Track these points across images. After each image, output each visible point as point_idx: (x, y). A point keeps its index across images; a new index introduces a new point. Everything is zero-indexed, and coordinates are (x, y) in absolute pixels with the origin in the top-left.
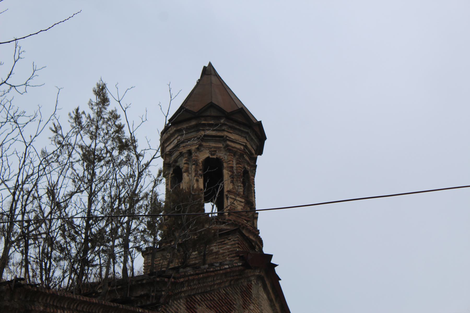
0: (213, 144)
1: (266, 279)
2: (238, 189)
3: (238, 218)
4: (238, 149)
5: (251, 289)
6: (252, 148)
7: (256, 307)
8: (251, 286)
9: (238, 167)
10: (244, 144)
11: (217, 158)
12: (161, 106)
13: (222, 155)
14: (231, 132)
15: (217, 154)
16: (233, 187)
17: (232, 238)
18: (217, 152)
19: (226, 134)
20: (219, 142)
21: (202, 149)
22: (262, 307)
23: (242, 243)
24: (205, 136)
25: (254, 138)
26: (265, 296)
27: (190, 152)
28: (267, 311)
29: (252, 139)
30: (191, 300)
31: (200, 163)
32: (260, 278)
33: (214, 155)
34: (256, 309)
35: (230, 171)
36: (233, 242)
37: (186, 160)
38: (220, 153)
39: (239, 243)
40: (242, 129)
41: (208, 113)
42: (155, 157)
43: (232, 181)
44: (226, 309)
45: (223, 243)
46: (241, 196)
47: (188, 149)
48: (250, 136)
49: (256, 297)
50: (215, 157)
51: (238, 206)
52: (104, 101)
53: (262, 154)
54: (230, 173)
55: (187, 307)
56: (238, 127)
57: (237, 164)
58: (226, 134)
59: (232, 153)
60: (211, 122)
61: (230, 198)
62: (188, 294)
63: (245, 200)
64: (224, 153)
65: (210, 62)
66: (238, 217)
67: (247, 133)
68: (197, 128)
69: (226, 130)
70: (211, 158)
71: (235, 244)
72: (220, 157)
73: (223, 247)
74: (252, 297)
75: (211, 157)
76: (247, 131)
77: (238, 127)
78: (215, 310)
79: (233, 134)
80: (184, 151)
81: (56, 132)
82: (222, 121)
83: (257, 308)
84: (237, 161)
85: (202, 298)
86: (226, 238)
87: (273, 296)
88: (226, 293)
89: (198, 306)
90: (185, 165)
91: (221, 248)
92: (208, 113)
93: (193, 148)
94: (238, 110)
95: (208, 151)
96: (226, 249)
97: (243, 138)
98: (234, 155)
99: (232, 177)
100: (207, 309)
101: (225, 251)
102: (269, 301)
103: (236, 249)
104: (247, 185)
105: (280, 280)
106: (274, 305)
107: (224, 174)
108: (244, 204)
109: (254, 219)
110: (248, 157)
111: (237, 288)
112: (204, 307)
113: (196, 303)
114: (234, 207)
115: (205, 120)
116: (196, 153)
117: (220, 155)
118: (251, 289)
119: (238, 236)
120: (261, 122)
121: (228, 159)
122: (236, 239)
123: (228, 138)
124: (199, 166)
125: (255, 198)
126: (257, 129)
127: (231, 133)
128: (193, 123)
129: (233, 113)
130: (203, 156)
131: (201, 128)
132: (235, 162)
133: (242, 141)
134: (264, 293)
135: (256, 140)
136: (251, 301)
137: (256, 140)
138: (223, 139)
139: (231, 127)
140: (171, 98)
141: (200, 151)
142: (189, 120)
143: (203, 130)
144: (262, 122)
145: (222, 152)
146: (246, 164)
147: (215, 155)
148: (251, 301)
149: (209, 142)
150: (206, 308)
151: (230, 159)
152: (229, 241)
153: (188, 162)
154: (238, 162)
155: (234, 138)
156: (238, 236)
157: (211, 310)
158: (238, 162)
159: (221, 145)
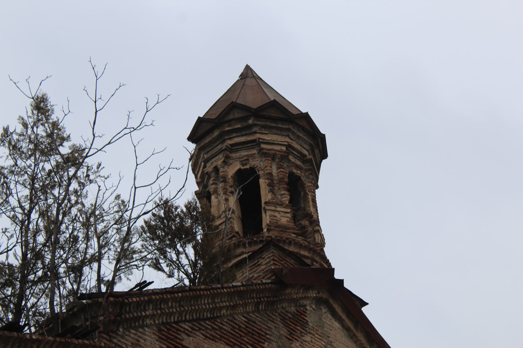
0: (244, 153)
1: (331, 302)
2: (281, 198)
3: (283, 233)
5: (306, 316)
6: (302, 148)
7: (318, 338)
8: (306, 313)
9: (279, 172)
10: (286, 144)
11: (250, 167)
12: (86, 91)
13: (257, 162)
14: (267, 132)
15: (250, 163)
16: (272, 197)
17: (266, 256)
18: (250, 160)
19: (258, 136)
20: (252, 148)
21: (231, 161)
22: (330, 339)
23: (282, 259)
24: (232, 145)
25: (301, 135)
26: (337, 325)
27: (216, 169)
28: (343, 344)
29: (299, 137)
30: (168, 329)
31: (230, 179)
32: (319, 302)
33: (246, 164)
34: (317, 341)
35: (268, 179)
36: (268, 260)
37: (213, 180)
38: (254, 161)
39: (276, 259)
40: (280, 126)
41: (231, 117)
43: (270, 189)
44: (247, 341)
46: (285, 206)
47: (214, 166)
48: (293, 133)
49: (317, 326)
50: (248, 167)
51: (282, 218)
53: (327, 156)
54: (267, 181)
55: (160, 337)
56: (273, 125)
57: (278, 168)
58: (258, 136)
59: (268, 157)
60: (236, 127)
61: (269, 210)
62: (163, 322)
63: (291, 209)
64: (259, 160)
66: (281, 231)
67: (289, 130)
68: (221, 138)
69: (258, 131)
70: (243, 169)
71: (269, 262)
72: (254, 165)
73: (257, 270)
74: (307, 326)
75: (242, 168)
76: (287, 127)
77: (273, 125)
78: (225, 342)
79: (269, 135)
82: (250, 122)
83: (320, 339)
84: (278, 165)
85: (193, 326)
86: (261, 257)
88: (248, 319)
89: (185, 337)
90: (212, 186)
91: (254, 272)
92: (231, 117)
93: (220, 163)
94: (270, 102)
96: (260, 271)
97: (283, 137)
98: (273, 159)
99: (271, 185)
100: (206, 341)
101: (260, 274)
102: (345, 331)
103: (271, 267)
104: (302, 195)
105: (365, 304)
106: (354, 335)
107: (260, 184)
108: (291, 215)
110: (299, 160)
111: (273, 314)
112: (198, 338)
113: (181, 333)
114: (277, 220)
116: (223, 168)
117: (255, 163)
118: (306, 316)
119: (272, 250)
121: (264, 165)
122: (270, 255)
123: (261, 140)
124: (229, 182)
125: (315, 207)
126: (303, 123)
127: (266, 134)
128: (216, 133)
129: (262, 108)
131: (226, 137)
132: (274, 167)
134: (333, 320)
135: (305, 137)
136: (306, 331)
137: (305, 137)
138: (256, 143)
140: (97, 77)
141: (229, 164)
142: (210, 131)
143: (230, 139)
144: (309, 113)
145: (256, 160)
146: (294, 168)
147: (248, 165)
148: (306, 331)
149: (239, 152)
150: (204, 339)
151: (266, 164)
152: (263, 260)
153: (215, 182)
154: (279, 166)
155: (269, 139)
156: (272, 250)
157: (216, 341)
158: (279, 166)
159: (255, 151)
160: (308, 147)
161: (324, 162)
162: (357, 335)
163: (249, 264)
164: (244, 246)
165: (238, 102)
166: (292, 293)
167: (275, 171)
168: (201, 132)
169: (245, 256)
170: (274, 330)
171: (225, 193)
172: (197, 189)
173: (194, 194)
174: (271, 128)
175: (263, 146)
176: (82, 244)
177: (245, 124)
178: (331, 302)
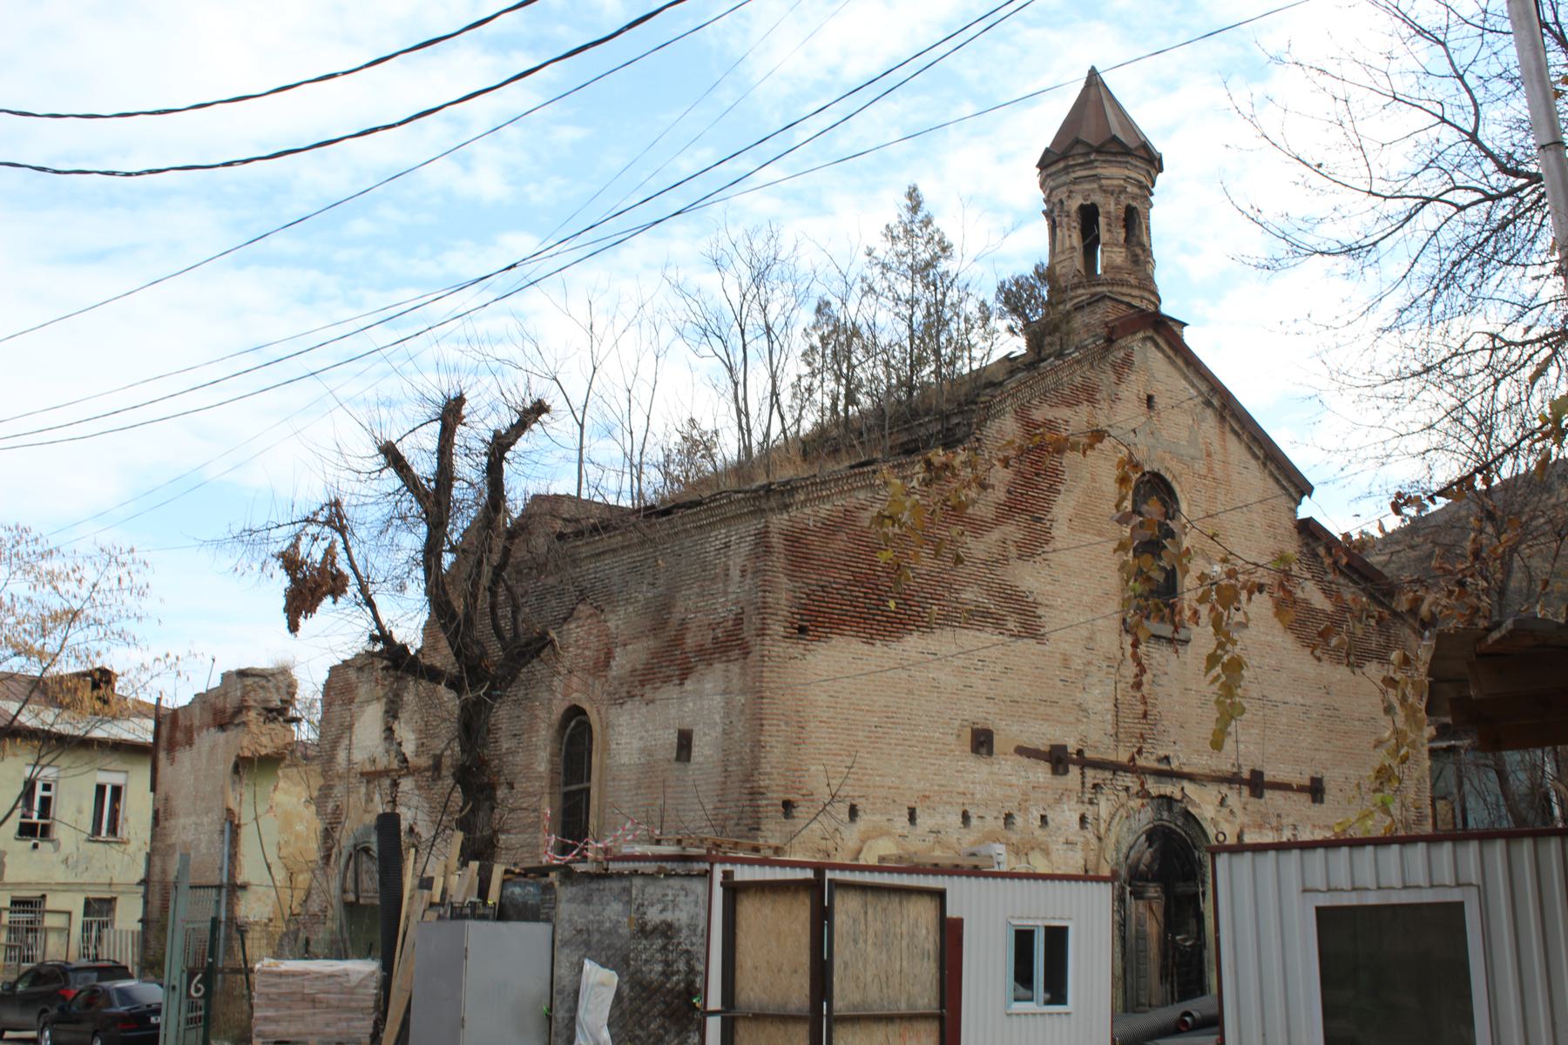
0: (1087, 186)
1: (1156, 337)
4: (1116, 186)
13: (1097, 198)
20: (1093, 181)
24: (1075, 178)
26: (1160, 355)
42: (580, 422)
45: (1093, 312)
48: (1132, 164)
50: (1089, 202)
52: (915, 207)
67: (1127, 162)
68: (1066, 170)
81: (869, 255)
82: (1092, 157)
87: (1171, 353)
95: (1080, 197)
98: (1112, 194)
109: (1051, 268)
115: (1074, 160)
138: (1097, 178)
139: (1105, 161)
143: (1074, 172)
160: (1144, 173)
162: (1063, 508)
163: (1087, 310)
164: (1084, 287)
165: (1102, 75)
166: (1122, 342)
168: (1047, 162)
169: (1083, 298)
170: (1105, 381)
171: (1069, 229)
174: (1110, 162)
175: (1104, 182)
177: (1088, 159)
178: (1156, 337)
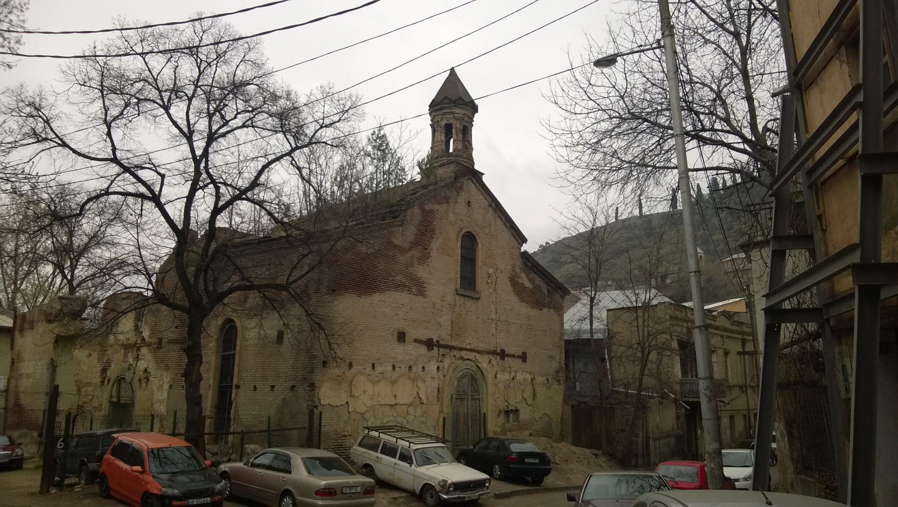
13: (452, 121)
26: (473, 186)
27: (438, 121)
41: (444, 102)
45: (449, 167)
65: (453, 80)
68: (441, 109)
80: (436, 121)
84: (158, 450)
85: (451, 111)
87: (477, 184)
92: (444, 102)
120: (58, 385)
130: (444, 122)
133: (89, 424)
138: (453, 113)
161: (476, 115)
167: (458, 126)
172: (431, 123)
173: (405, 331)
176: (292, 157)
